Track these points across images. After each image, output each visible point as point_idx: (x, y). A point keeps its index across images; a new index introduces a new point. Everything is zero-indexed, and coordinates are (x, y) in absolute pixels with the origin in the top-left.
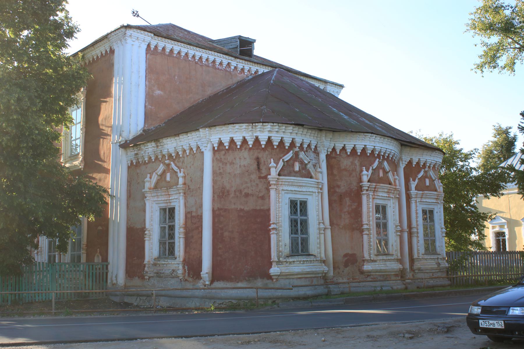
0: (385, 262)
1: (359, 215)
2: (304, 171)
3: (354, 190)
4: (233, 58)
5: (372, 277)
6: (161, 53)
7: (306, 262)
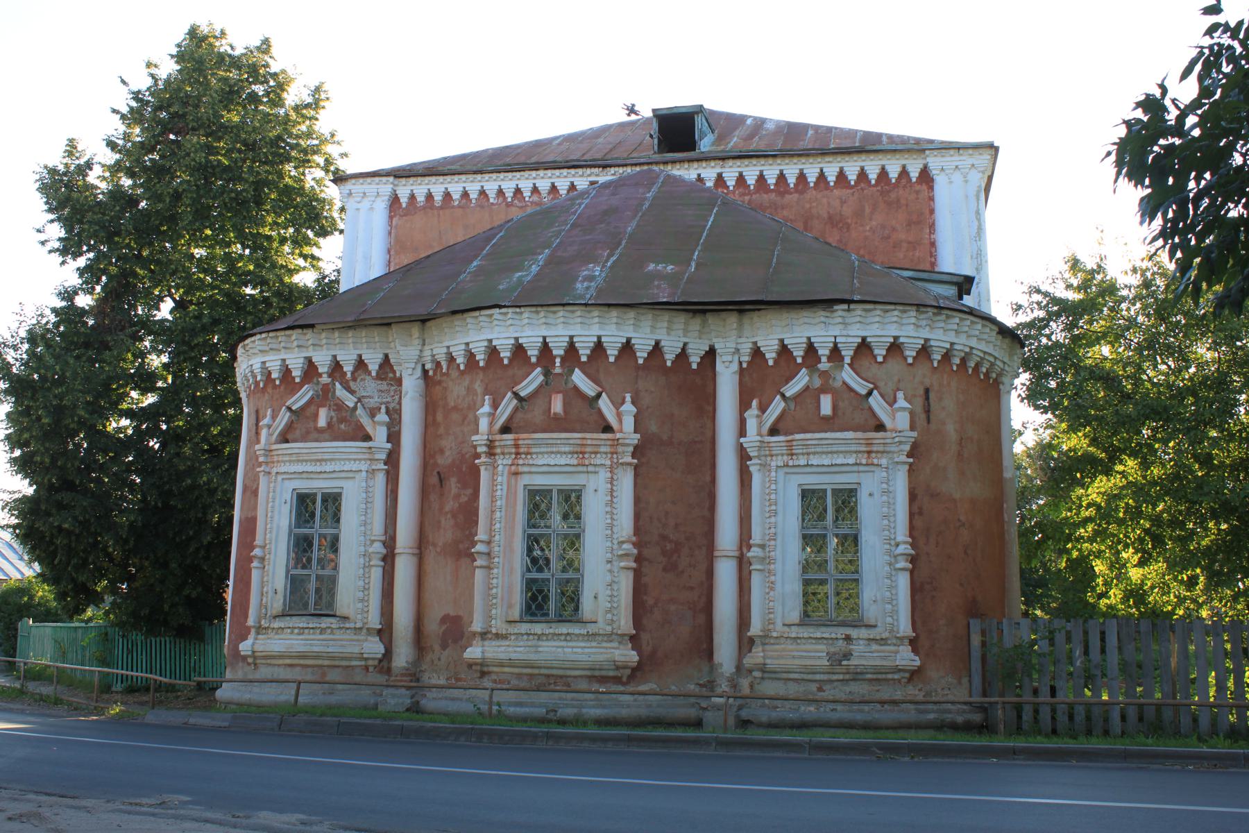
0: (539, 639)
2: (342, 426)
3: (467, 456)
4: (596, 170)
5: (494, 677)
6: (424, 208)
7: (306, 631)
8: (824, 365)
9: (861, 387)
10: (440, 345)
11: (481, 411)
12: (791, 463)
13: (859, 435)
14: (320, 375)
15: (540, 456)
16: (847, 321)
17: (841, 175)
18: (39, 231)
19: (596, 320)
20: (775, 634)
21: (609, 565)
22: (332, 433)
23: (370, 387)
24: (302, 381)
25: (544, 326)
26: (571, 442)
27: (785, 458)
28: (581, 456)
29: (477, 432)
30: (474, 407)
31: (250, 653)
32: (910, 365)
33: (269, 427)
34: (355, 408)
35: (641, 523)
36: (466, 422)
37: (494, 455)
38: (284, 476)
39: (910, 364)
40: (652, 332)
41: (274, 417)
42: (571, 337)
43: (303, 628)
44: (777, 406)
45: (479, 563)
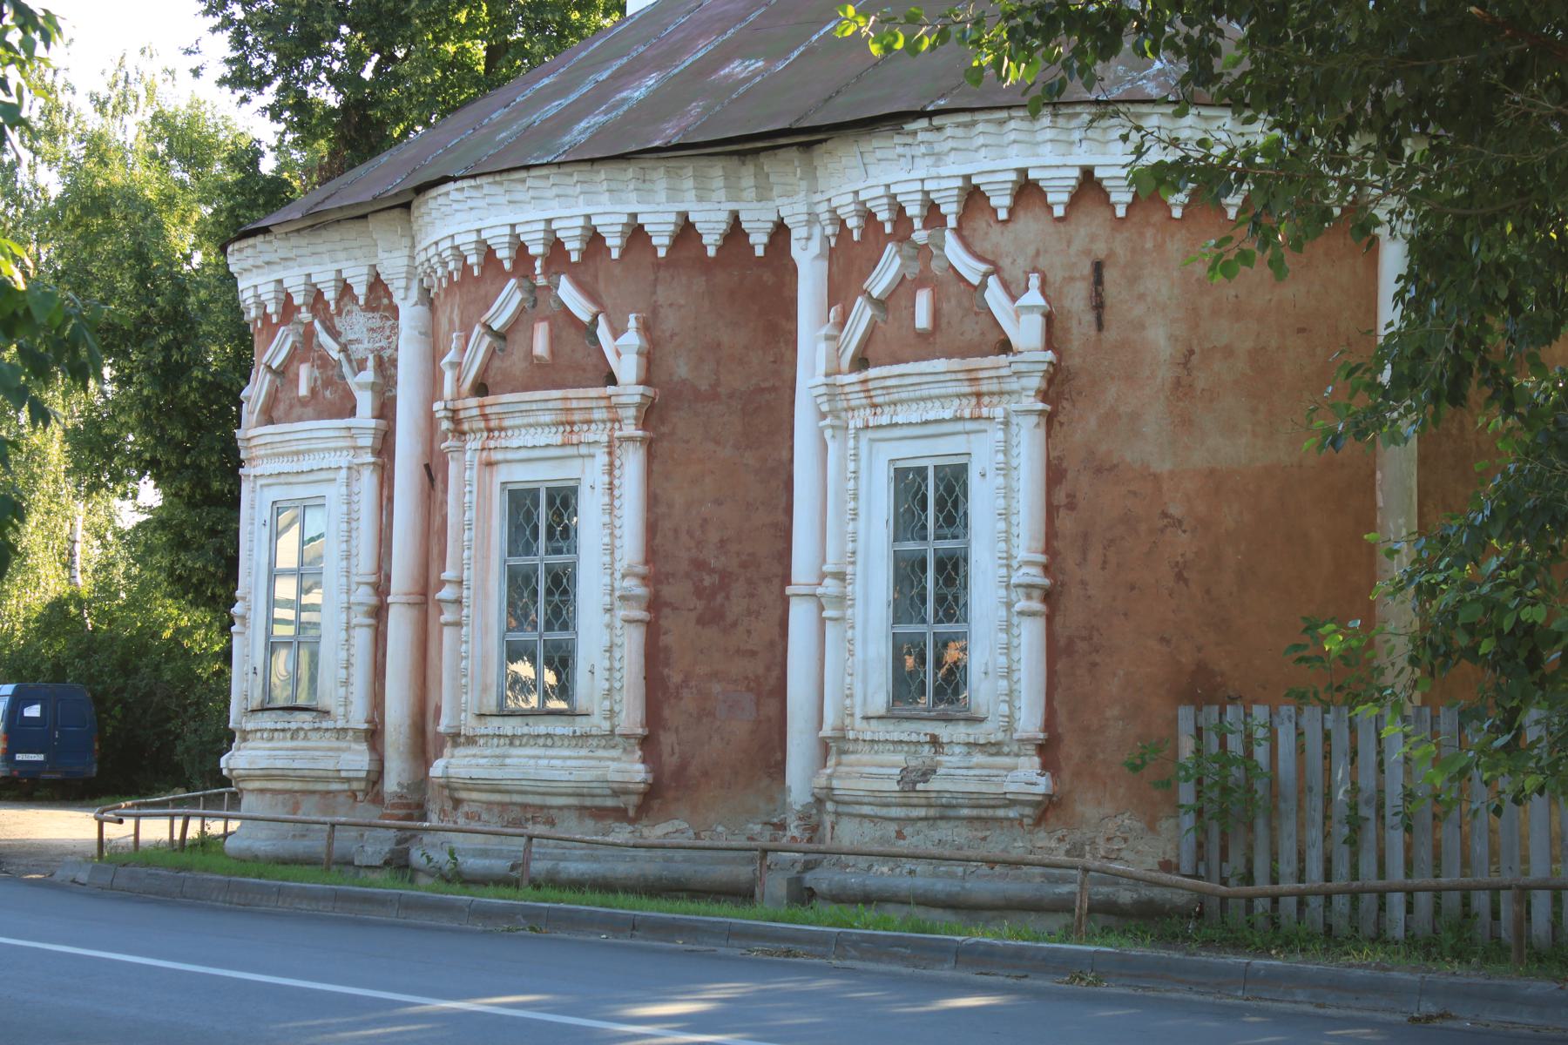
0: (511, 744)
2: (328, 393)
8: (920, 236)
13: (955, 364)
16: (937, 148)
18: (189, 52)
19: (605, 186)
21: (608, 616)
23: (357, 325)
26: (550, 405)
28: (568, 428)
32: (1060, 219)
34: (984, 285)
35: (658, 540)
37: (464, 433)
40: (669, 200)
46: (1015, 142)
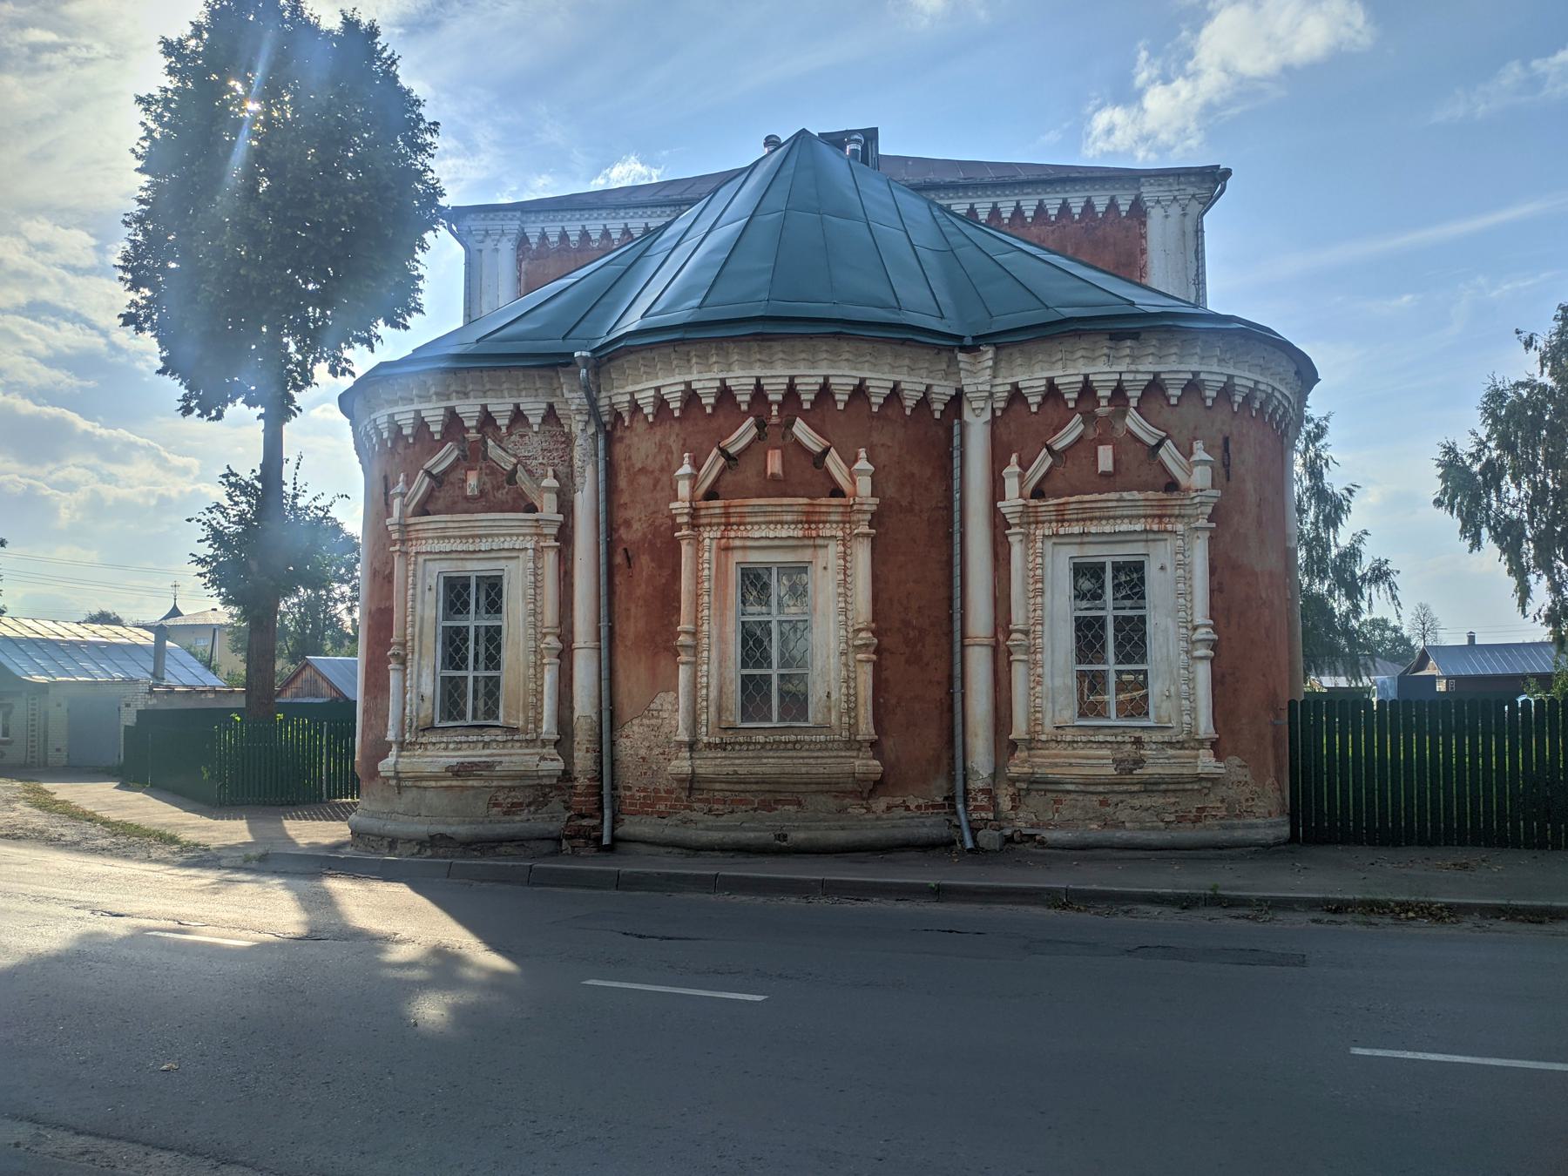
1: (677, 605)
3: (662, 529)
7: (465, 746)
8: (1103, 409)
9: (1148, 435)
10: (621, 391)
11: (680, 472)
12: (1062, 531)
14: (467, 430)
15: (756, 527)
17: (1041, 210)
20: (1044, 737)
22: (484, 502)
24: (442, 437)
25: (758, 364)
27: (1054, 524)
28: (806, 526)
29: (676, 498)
30: (669, 468)
31: (392, 774)
33: (403, 495)
36: (658, 488)
37: (699, 526)
38: (428, 557)
39: (1210, 408)
41: (409, 483)
42: (792, 378)
43: (461, 742)
44: (1042, 463)
45: (683, 658)
46: (804, 359)
